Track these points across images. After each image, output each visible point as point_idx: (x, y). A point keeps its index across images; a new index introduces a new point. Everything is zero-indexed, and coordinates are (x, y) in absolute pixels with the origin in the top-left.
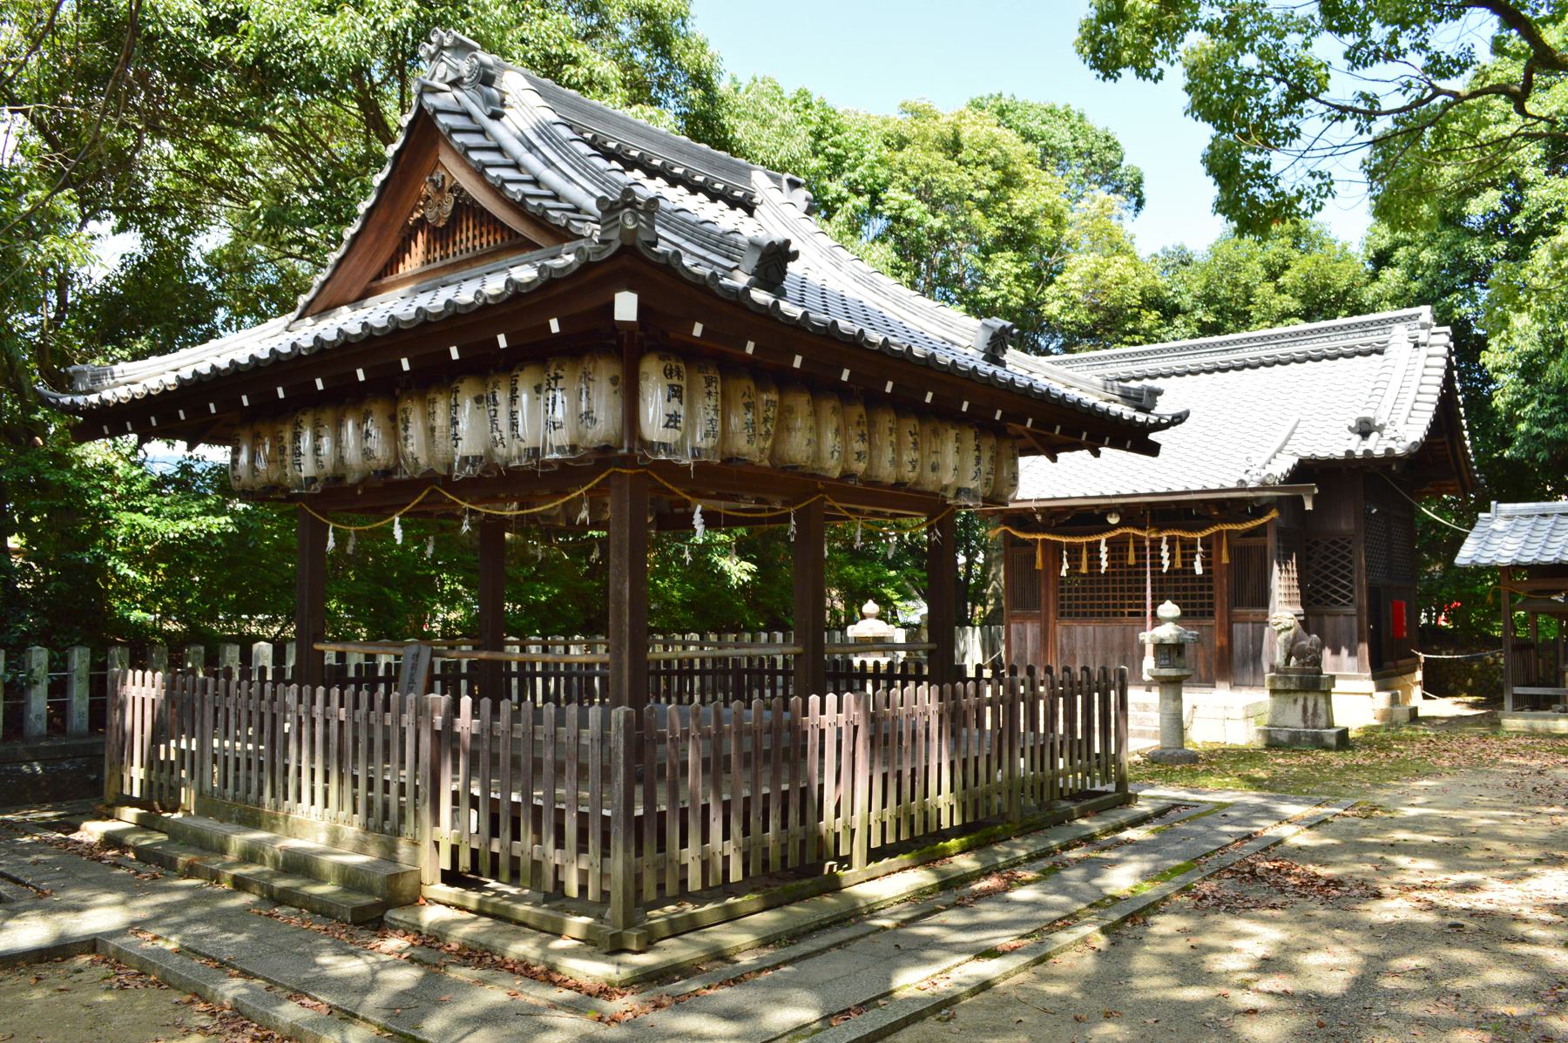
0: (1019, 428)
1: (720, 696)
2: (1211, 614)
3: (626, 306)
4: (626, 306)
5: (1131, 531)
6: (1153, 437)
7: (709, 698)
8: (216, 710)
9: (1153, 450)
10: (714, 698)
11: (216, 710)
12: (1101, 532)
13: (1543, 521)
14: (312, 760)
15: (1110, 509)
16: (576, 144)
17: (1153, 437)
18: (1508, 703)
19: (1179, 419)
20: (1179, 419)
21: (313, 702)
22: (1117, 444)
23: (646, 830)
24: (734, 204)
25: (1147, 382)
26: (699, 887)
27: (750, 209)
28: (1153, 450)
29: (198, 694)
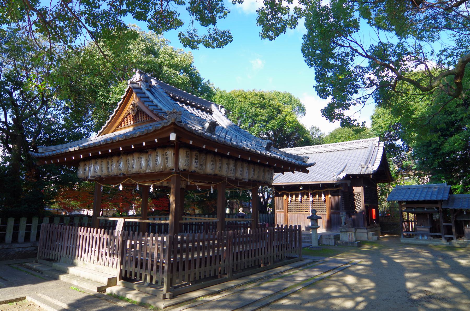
0: (158, 183)
1: (199, 231)
2: (325, 212)
3: (173, 137)
4: (173, 137)
5: (306, 191)
6: (307, 169)
7: (197, 231)
8: (69, 234)
9: (307, 172)
10: (198, 232)
11: (69, 234)
12: (121, 216)
13: (409, 190)
14: (92, 247)
15: (299, 186)
16: (167, 97)
17: (307, 169)
18: (402, 237)
19: (313, 165)
20: (313, 165)
21: (93, 232)
22: (298, 170)
23: (174, 266)
24: (207, 112)
25: (305, 155)
26: (198, 279)
27: (211, 114)
28: (307, 172)
29: (64, 230)
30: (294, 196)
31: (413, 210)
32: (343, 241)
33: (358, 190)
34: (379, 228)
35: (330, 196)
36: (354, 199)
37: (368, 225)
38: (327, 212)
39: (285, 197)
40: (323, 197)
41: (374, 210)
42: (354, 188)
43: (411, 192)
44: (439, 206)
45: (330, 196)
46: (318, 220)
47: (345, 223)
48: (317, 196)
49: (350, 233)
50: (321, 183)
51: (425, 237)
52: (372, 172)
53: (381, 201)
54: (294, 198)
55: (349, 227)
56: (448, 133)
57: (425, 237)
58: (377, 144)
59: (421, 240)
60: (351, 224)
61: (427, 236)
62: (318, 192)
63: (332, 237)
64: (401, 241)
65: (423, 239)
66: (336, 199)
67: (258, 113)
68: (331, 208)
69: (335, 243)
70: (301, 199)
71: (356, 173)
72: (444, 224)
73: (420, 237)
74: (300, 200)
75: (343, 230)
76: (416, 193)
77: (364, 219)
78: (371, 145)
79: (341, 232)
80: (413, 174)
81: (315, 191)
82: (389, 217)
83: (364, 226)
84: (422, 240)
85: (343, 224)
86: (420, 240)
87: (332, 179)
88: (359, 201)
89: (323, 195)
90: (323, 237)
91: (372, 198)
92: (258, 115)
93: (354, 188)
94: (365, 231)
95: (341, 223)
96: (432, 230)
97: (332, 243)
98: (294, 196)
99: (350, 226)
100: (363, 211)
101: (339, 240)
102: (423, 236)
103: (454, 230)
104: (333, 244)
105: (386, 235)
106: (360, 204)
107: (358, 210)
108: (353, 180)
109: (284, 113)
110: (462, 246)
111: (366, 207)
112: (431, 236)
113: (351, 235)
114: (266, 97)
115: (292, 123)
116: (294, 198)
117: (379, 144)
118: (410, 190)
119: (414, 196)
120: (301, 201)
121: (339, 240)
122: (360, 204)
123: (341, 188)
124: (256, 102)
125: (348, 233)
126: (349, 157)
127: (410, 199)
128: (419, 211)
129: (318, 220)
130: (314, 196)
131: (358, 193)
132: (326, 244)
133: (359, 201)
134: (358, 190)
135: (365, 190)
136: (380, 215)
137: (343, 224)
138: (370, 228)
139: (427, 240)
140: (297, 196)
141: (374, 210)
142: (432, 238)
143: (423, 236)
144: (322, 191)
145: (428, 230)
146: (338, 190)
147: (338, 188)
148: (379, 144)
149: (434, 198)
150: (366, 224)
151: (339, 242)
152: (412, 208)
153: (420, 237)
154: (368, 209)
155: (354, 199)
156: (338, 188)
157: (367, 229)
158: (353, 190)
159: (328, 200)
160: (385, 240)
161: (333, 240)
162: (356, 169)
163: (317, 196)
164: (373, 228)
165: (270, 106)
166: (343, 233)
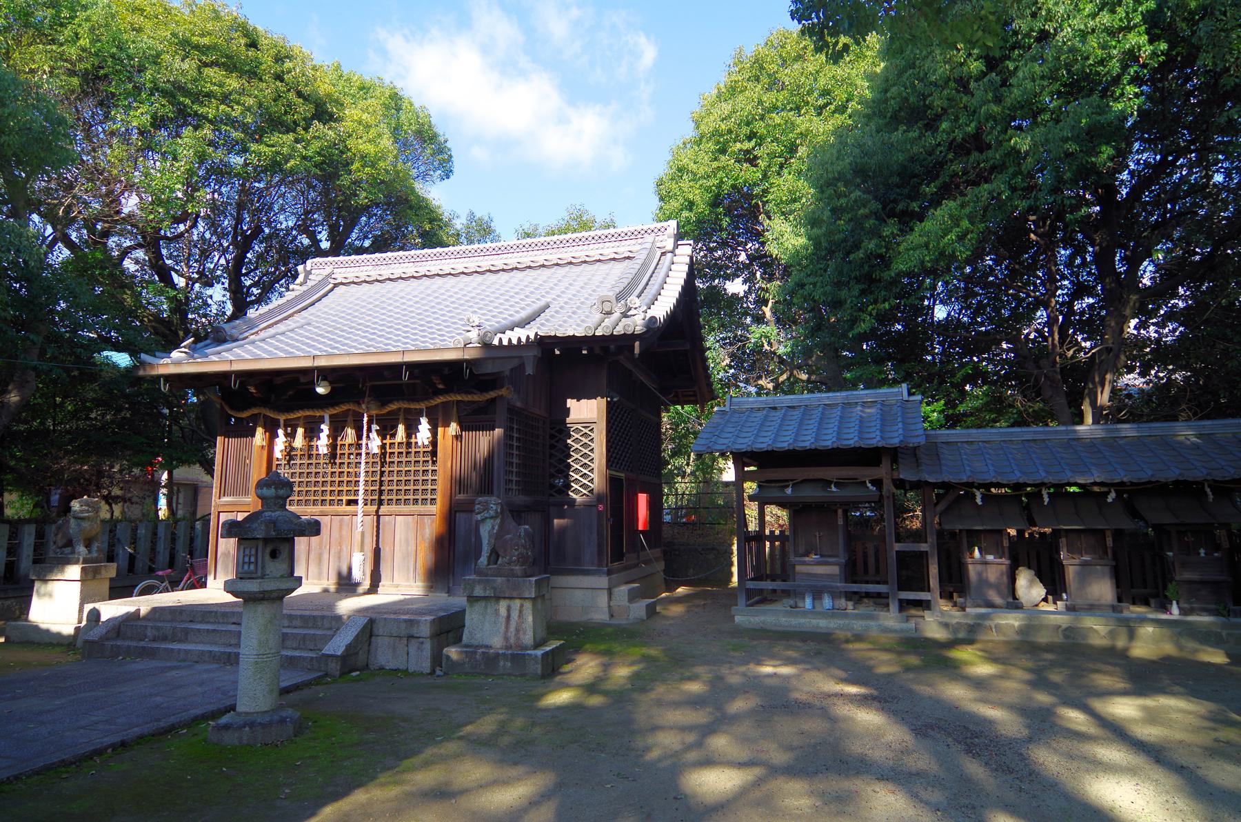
5: (352, 407)
13: (773, 413)
30: (300, 431)
31: (789, 491)
32: (471, 650)
33: (586, 412)
34: (660, 566)
35: (453, 428)
36: (568, 447)
37: (618, 555)
38: (438, 497)
39: (260, 437)
40: (424, 432)
41: (643, 499)
42: (571, 403)
43: (783, 420)
44: (882, 471)
45: (453, 428)
46: (301, 543)
47: (495, 555)
48: (401, 428)
49: (518, 603)
50: (409, 358)
51: (827, 602)
52: (639, 329)
53: (671, 475)
54: (299, 441)
55: (512, 574)
56: (915, 206)
57: (827, 602)
58: (669, 244)
59: (813, 615)
60: (523, 559)
61: (835, 595)
62: (407, 411)
63: (425, 630)
64: (738, 619)
65: (818, 609)
66: (484, 442)
67: (209, 87)
68: (459, 484)
69: (437, 658)
70: (333, 446)
71: (580, 332)
72: (898, 547)
73: (808, 603)
74: (323, 450)
75: (478, 591)
76: (801, 424)
77: (600, 535)
78: (648, 246)
79: (472, 599)
80: (770, 386)
81: (393, 406)
82: (694, 524)
83: (600, 564)
84: (813, 613)
85: (483, 560)
86: (805, 613)
87: (460, 340)
88: (585, 456)
89: (424, 426)
90: (380, 629)
91: (634, 450)
92: (209, 95)
93: (571, 403)
94: (603, 581)
95: (478, 556)
96: (853, 571)
97: (420, 659)
98: (300, 431)
99: (517, 569)
100: (600, 498)
101: (458, 640)
102: (817, 595)
103: (934, 570)
104: (426, 666)
105: (681, 590)
106: (589, 470)
107: (578, 494)
108: (566, 363)
109: (347, 125)
110: (961, 635)
111: (613, 482)
112: (850, 596)
113: (515, 615)
114: (263, 42)
115: (373, 166)
116: (299, 441)
117: (676, 246)
118: (779, 414)
119: (797, 435)
120: (333, 455)
121: (458, 640)
122: (589, 470)
123: (503, 392)
124: (205, 41)
125: (502, 606)
126: (562, 287)
127: (785, 442)
128: (810, 493)
129: (301, 543)
130: (387, 430)
131: (586, 424)
132: (391, 665)
133: (585, 456)
134: (586, 412)
135: (611, 409)
136: (667, 518)
137: (483, 560)
138: (626, 568)
139: (833, 613)
140: (312, 433)
141: (643, 499)
142: (850, 605)
143: (817, 595)
144: (423, 406)
145: (835, 570)
146: (493, 400)
147: (492, 394)
148: (676, 246)
149: (874, 439)
150: (883, 601)
151: (453, 652)
152: (783, 483)
153: (808, 603)
154: (618, 493)
155: (566, 451)
156: (492, 394)
157: (609, 573)
158: (567, 412)
159: (446, 446)
160: (677, 610)
161: (428, 646)
162: (575, 319)
163: (401, 428)
164: (636, 565)
165: (279, 77)
166: (479, 607)
